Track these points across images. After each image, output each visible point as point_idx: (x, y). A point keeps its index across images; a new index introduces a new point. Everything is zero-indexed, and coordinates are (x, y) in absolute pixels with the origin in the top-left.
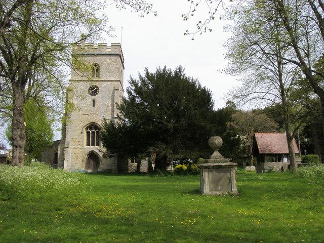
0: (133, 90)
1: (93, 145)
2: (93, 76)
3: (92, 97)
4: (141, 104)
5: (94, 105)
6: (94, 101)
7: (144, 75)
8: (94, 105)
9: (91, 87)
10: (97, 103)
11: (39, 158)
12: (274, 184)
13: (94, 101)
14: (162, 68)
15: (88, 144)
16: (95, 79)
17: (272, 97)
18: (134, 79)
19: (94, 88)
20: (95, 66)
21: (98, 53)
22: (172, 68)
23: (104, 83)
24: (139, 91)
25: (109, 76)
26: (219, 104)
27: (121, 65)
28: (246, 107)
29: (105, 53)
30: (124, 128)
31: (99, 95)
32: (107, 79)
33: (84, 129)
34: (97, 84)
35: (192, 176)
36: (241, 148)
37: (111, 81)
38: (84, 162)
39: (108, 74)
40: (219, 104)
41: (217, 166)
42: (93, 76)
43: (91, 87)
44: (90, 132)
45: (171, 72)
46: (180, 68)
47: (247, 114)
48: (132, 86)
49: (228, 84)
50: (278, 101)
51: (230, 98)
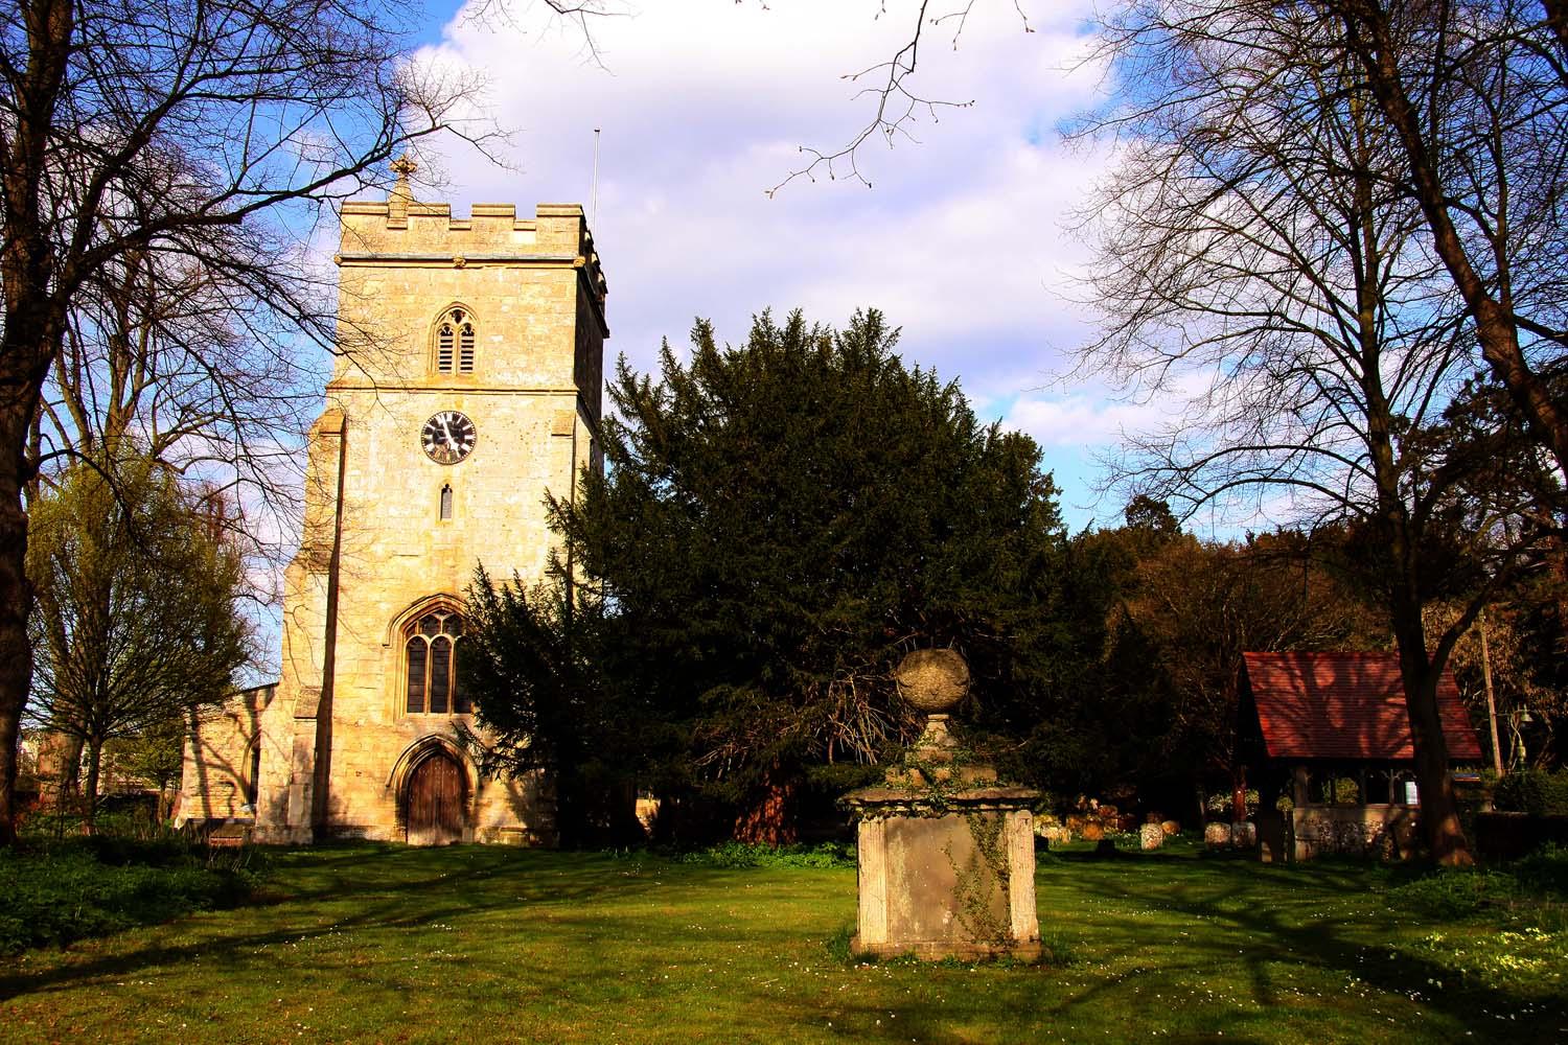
0: (633, 436)
2: (445, 365)
3: (439, 473)
4: (680, 507)
5: (444, 511)
7: (686, 356)
8: (444, 511)
14: (781, 324)
16: (453, 379)
17: (1333, 475)
18: (639, 381)
20: (458, 316)
22: (830, 315)
23: (498, 399)
26: (1085, 507)
27: (402, 274)
28: (1225, 521)
30: (581, 624)
31: (479, 457)
34: (468, 407)
36: (1551, 414)
40: (1085, 507)
42: (445, 365)
43: (464, 422)
44: (429, 641)
45: (825, 346)
47: (1221, 557)
48: (626, 413)
49: (1146, 394)
50: (1365, 488)
51: (1144, 483)
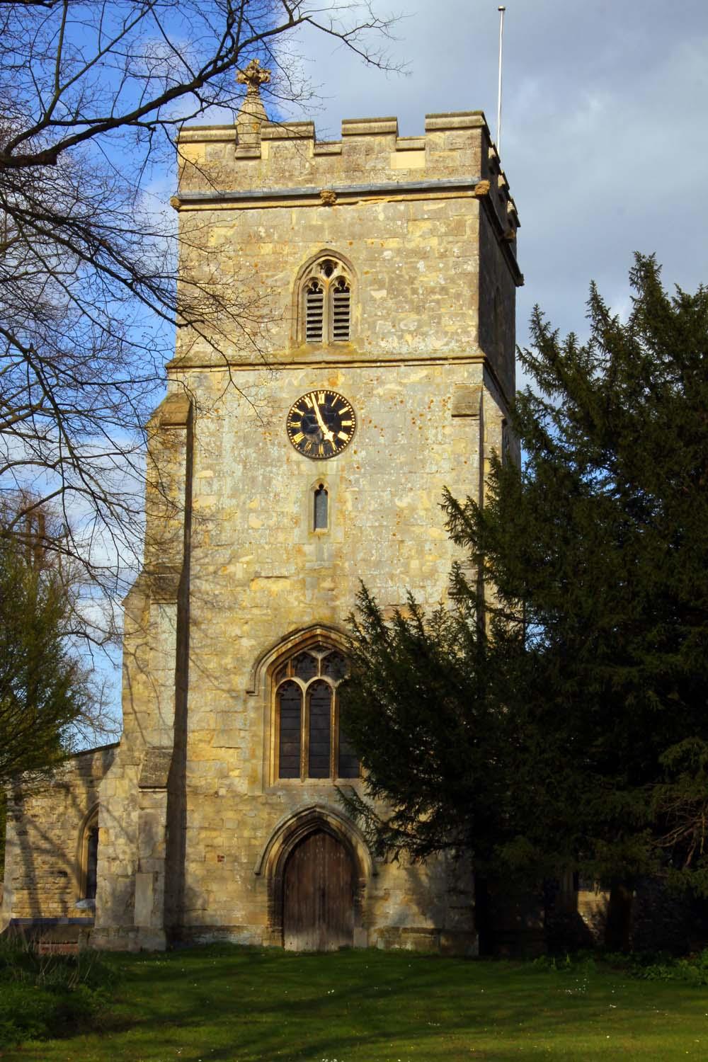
6: (320, 492)
7: (622, 309)
9: (341, 404)
10: (341, 501)
12: (230, 552)
13: (320, 492)
18: (561, 342)
19: (334, 421)
20: (328, 268)
21: (341, 184)
24: (599, 417)
25: (418, 332)
29: (392, 184)
30: (496, 657)
31: (357, 452)
32: (404, 351)
34: (342, 383)
37: (433, 360)
39: (411, 320)
43: (341, 404)
44: (304, 686)
46: (638, 257)
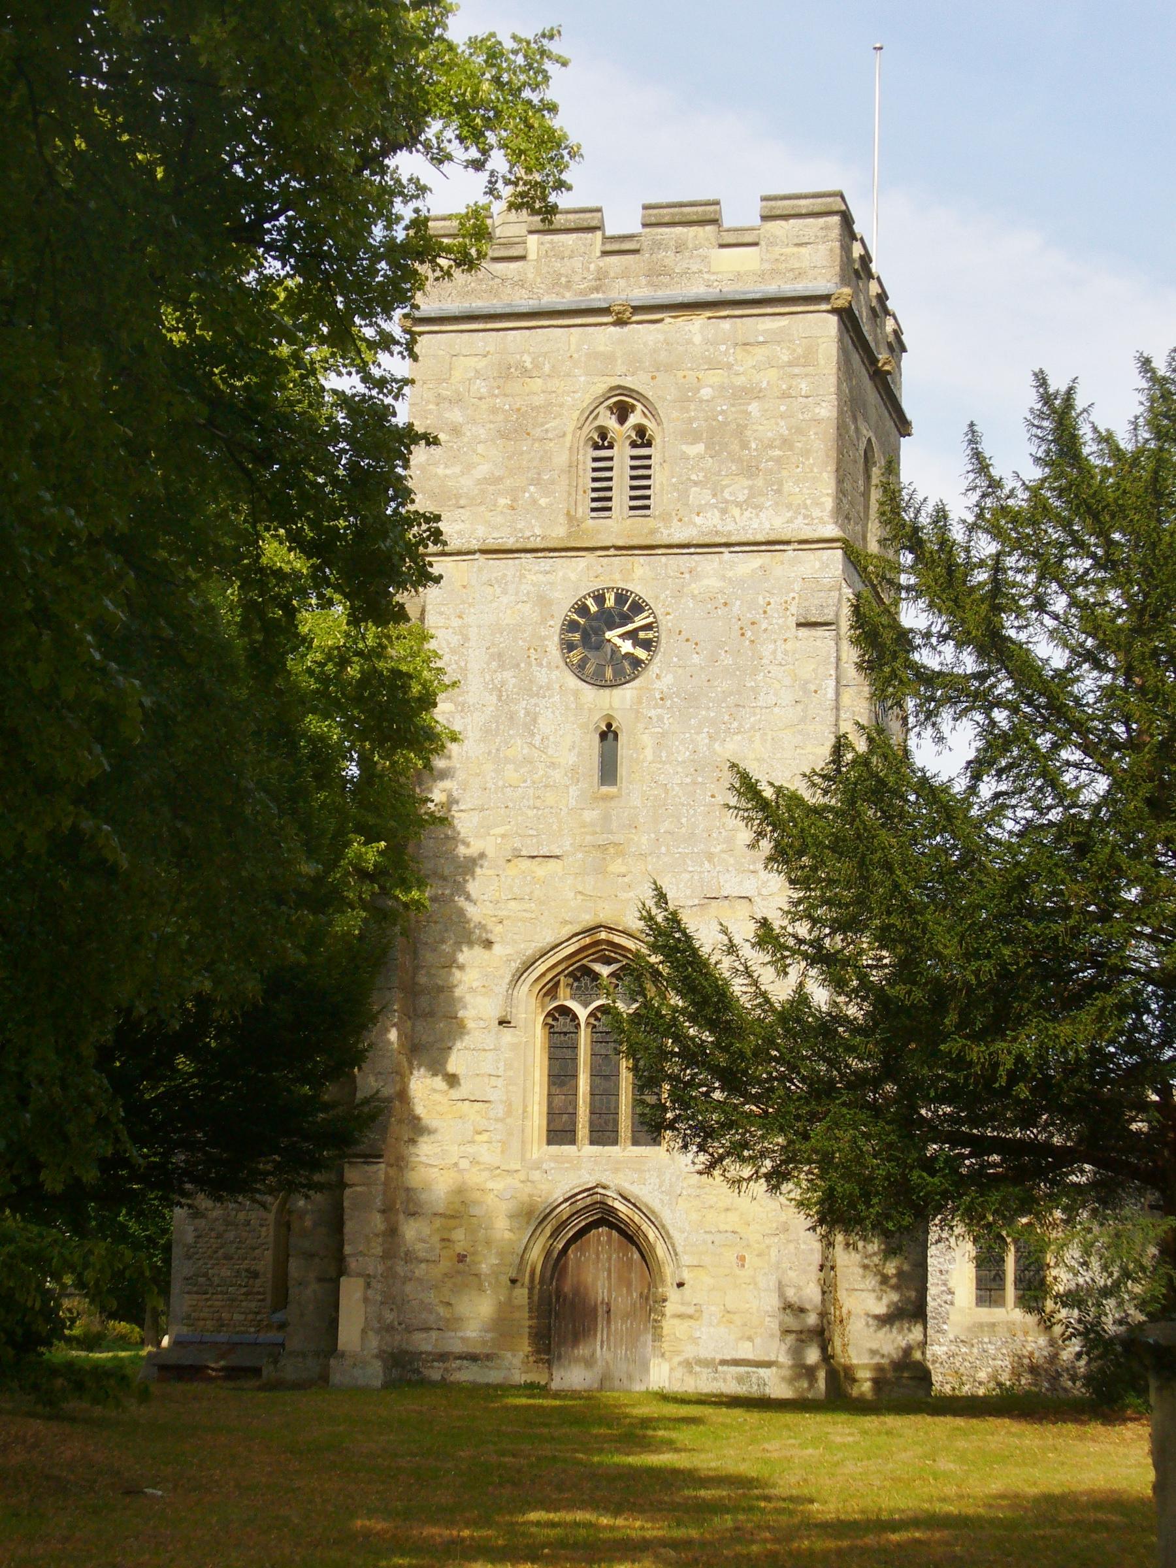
1: (603, 1134)
2: (602, 503)
5: (608, 771)
6: (608, 735)
7: (1020, 463)
8: (608, 771)
9: (582, 610)
11: (977, 1266)
13: (608, 735)
15: (560, 1132)
21: (641, 293)
31: (660, 675)
33: (526, 993)
34: (639, 577)
35: (1057, 1491)
37: (773, 544)
38: (521, 1294)
39: (738, 489)
41: (617, 1107)
42: (602, 503)
44: (582, 1013)
